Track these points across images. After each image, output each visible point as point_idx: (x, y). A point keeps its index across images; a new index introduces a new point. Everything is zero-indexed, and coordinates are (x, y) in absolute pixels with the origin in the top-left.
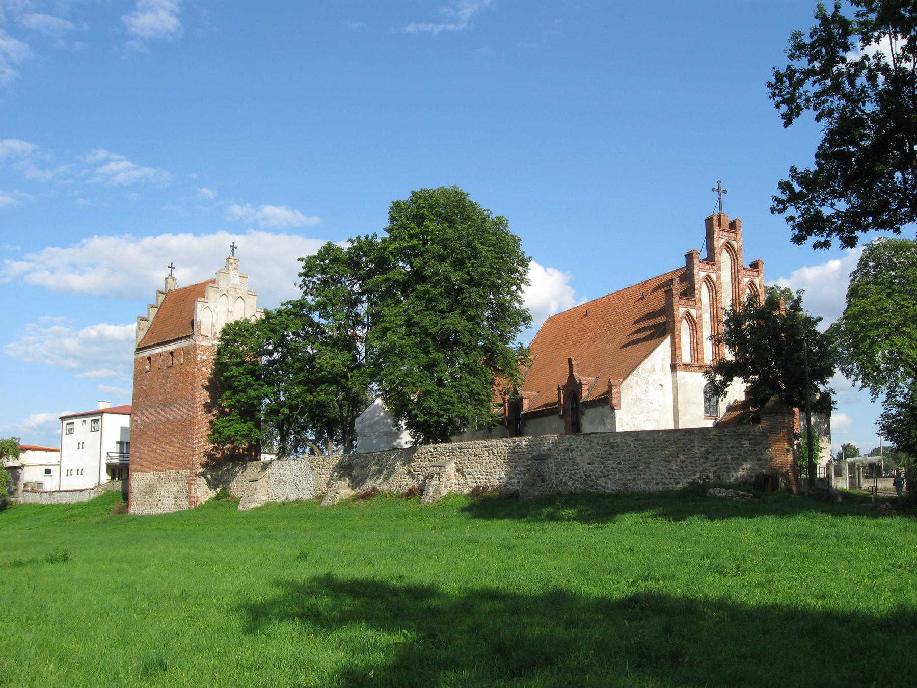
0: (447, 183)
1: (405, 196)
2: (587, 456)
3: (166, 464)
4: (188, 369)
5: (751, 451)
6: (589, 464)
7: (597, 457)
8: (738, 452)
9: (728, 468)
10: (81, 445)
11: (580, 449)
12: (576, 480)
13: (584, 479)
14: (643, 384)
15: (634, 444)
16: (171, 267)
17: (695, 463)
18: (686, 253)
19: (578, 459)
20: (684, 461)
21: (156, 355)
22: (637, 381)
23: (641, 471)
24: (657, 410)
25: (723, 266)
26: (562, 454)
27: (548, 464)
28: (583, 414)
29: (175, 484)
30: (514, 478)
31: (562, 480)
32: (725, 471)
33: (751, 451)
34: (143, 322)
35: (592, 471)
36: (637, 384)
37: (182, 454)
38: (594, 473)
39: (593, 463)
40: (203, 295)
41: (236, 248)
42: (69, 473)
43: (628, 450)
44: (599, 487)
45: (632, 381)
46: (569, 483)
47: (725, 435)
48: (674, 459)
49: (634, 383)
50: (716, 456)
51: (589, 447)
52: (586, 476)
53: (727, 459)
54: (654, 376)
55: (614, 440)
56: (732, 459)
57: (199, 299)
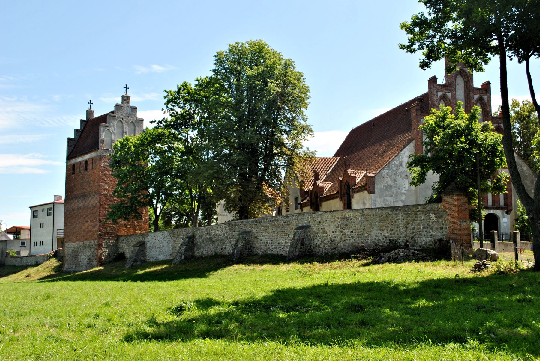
0: (255, 38)
1: (225, 49)
2: (332, 226)
3: (84, 236)
4: (96, 172)
5: (435, 222)
6: (333, 232)
7: (338, 227)
8: (427, 223)
9: (421, 235)
10: (42, 226)
11: (327, 222)
12: (326, 244)
13: (330, 243)
14: (393, 175)
15: (361, 218)
16: (90, 103)
17: (399, 231)
18: (428, 79)
19: (327, 228)
20: (393, 230)
21: (80, 162)
22: (388, 173)
23: (366, 237)
24: (404, 193)
25: (457, 87)
26: (317, 225)
27: (307, 233)
28: (353, 198)
29: (89, 250)
30: (288, 243)
31: (317, 244)
32: (418, 237)
33: (435, 222)
34: (71, 141)
35: (335, 237)
36: (388, 175)
37: (93, 230)
38: (336, 238)
39: (336, 232)
40: (105, 122)
41: (124, 88)
42: (35, 244)
43: (357, 222)
44: (340, 249)
45: (384, 173)
46: (322, 246)
47: (419, 211)
48: (386, 228)
49: (386, 175)
50: (413, 226)
51: (333, 220)
52: (331, 240)
53: (420, 228)
54: (401, 170)
55: (349, 215)
56: (424, 228)
57: (102, 124)
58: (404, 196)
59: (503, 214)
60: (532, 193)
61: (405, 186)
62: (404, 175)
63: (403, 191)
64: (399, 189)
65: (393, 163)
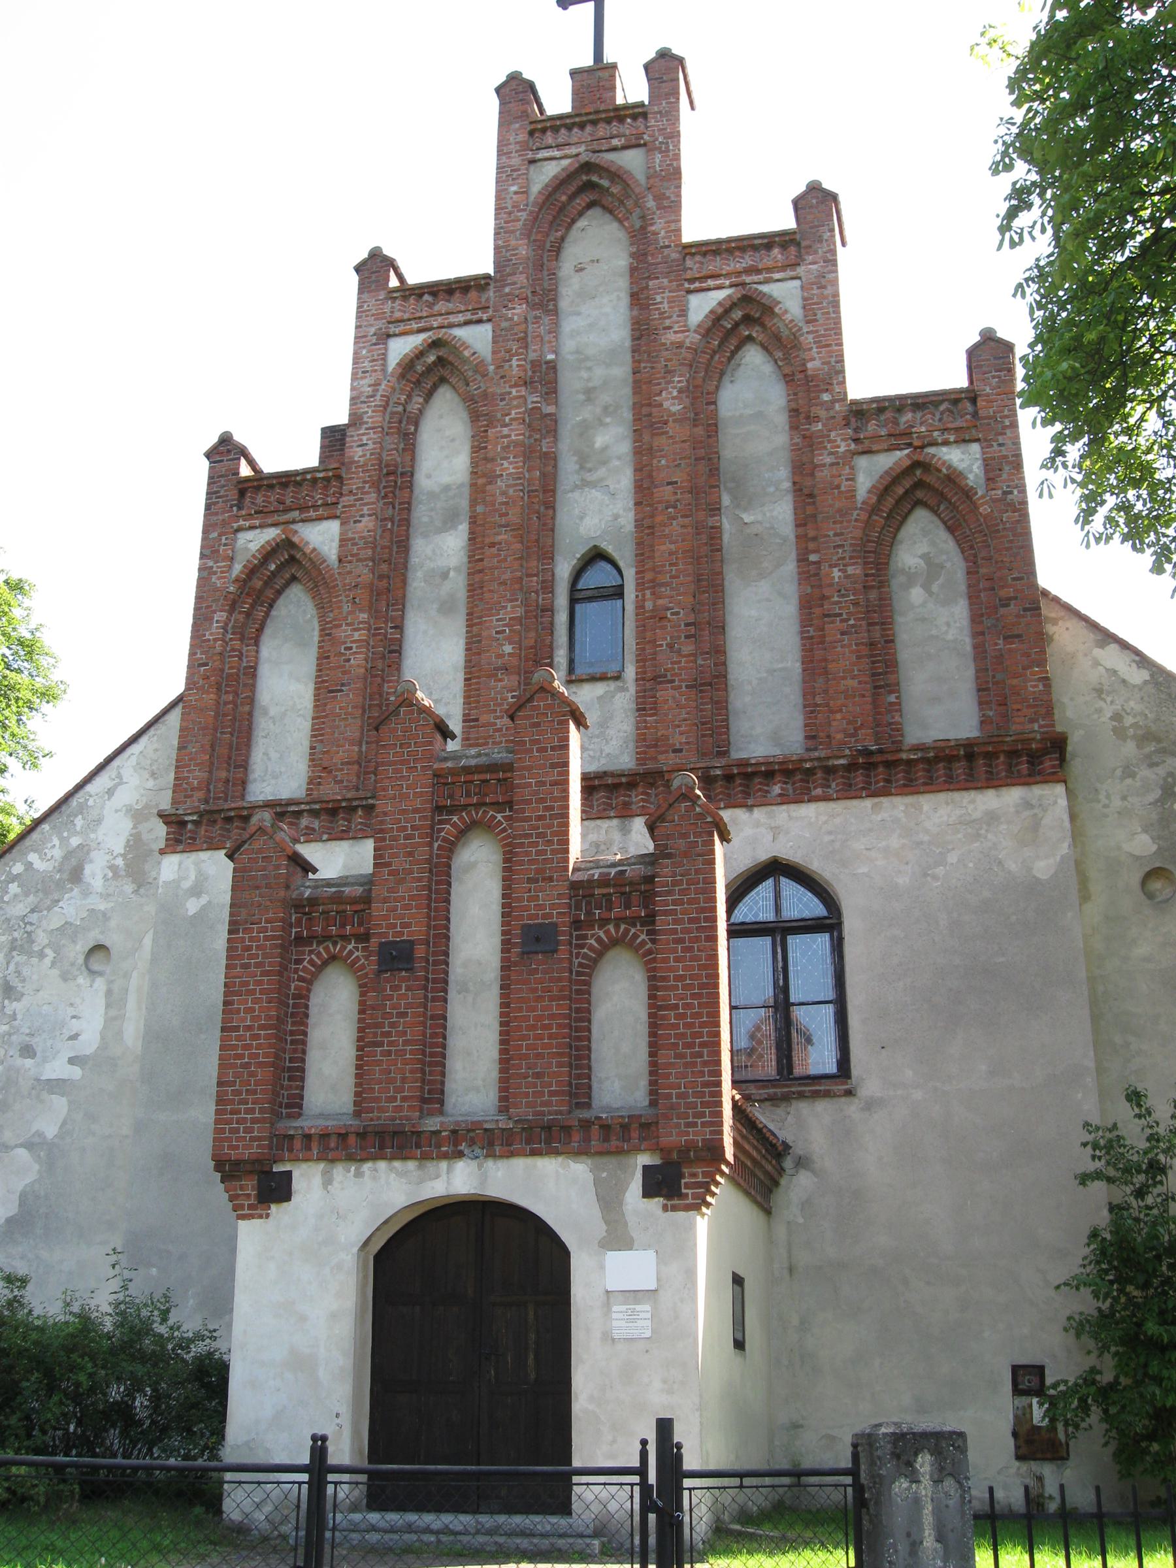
24: (57, 1086)
58: (60, 1104)
59: (610, 1202)
60: (392, 273)
61: (75, 1026)
62: (77, 951)
63: (58, 1069)
64: (27, 1051)
65: (18, 868)
